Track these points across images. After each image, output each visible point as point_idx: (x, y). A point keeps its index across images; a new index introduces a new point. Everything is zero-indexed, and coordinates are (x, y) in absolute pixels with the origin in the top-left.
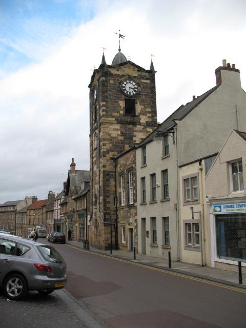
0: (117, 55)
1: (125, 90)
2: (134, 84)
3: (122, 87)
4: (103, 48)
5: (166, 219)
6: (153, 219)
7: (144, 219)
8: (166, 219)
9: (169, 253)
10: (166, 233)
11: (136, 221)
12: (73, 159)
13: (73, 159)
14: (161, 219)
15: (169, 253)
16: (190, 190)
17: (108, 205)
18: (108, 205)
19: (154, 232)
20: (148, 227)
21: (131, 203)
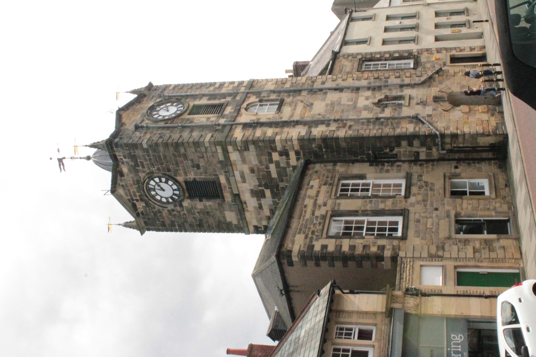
0: (97, 163)
1: (166, 182)
2: (158, 198)
3: (149, 190)
4: (74, 146)
5: (437, 14)
6: (437, 26)
7: (437, 39)
8: (437, 14)
9: (474, 22)
10: (453, 13)
11: (439, 51)
12: (229, 352)
13: (229, 352)
14: (436, 30)
15: (474, 22)
16: (385, 69)
17: (404, 143)
18: (404, 143)
19: (453, 26)
20: (447, 31)
21: (411, 63)
